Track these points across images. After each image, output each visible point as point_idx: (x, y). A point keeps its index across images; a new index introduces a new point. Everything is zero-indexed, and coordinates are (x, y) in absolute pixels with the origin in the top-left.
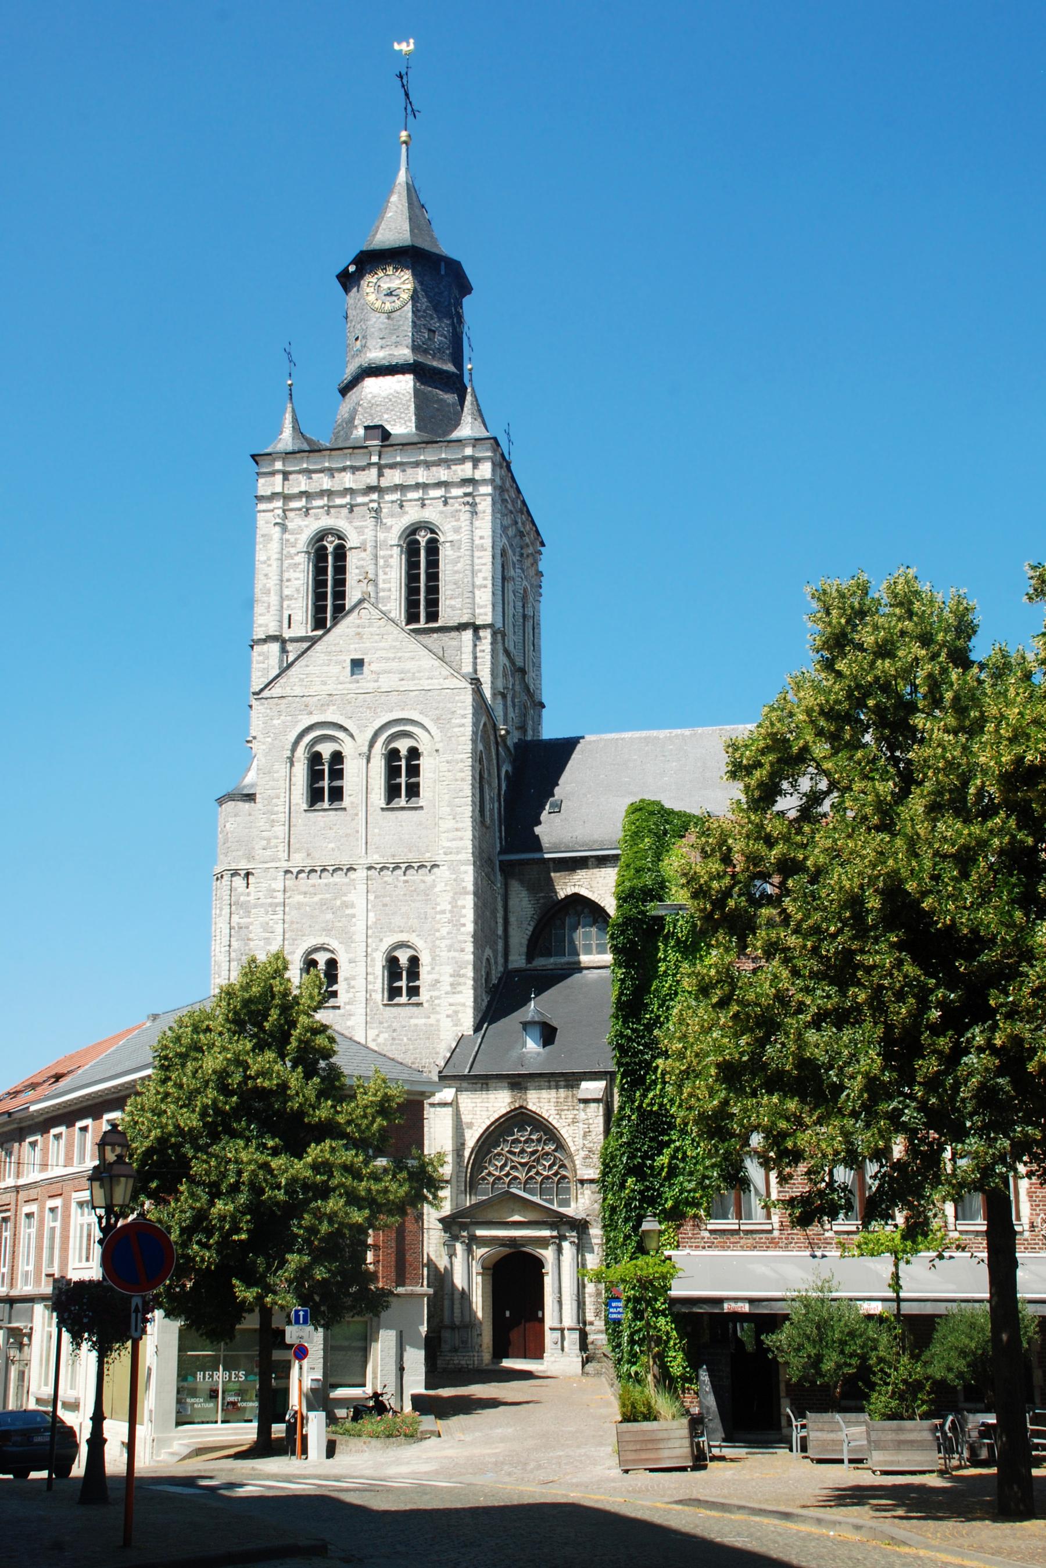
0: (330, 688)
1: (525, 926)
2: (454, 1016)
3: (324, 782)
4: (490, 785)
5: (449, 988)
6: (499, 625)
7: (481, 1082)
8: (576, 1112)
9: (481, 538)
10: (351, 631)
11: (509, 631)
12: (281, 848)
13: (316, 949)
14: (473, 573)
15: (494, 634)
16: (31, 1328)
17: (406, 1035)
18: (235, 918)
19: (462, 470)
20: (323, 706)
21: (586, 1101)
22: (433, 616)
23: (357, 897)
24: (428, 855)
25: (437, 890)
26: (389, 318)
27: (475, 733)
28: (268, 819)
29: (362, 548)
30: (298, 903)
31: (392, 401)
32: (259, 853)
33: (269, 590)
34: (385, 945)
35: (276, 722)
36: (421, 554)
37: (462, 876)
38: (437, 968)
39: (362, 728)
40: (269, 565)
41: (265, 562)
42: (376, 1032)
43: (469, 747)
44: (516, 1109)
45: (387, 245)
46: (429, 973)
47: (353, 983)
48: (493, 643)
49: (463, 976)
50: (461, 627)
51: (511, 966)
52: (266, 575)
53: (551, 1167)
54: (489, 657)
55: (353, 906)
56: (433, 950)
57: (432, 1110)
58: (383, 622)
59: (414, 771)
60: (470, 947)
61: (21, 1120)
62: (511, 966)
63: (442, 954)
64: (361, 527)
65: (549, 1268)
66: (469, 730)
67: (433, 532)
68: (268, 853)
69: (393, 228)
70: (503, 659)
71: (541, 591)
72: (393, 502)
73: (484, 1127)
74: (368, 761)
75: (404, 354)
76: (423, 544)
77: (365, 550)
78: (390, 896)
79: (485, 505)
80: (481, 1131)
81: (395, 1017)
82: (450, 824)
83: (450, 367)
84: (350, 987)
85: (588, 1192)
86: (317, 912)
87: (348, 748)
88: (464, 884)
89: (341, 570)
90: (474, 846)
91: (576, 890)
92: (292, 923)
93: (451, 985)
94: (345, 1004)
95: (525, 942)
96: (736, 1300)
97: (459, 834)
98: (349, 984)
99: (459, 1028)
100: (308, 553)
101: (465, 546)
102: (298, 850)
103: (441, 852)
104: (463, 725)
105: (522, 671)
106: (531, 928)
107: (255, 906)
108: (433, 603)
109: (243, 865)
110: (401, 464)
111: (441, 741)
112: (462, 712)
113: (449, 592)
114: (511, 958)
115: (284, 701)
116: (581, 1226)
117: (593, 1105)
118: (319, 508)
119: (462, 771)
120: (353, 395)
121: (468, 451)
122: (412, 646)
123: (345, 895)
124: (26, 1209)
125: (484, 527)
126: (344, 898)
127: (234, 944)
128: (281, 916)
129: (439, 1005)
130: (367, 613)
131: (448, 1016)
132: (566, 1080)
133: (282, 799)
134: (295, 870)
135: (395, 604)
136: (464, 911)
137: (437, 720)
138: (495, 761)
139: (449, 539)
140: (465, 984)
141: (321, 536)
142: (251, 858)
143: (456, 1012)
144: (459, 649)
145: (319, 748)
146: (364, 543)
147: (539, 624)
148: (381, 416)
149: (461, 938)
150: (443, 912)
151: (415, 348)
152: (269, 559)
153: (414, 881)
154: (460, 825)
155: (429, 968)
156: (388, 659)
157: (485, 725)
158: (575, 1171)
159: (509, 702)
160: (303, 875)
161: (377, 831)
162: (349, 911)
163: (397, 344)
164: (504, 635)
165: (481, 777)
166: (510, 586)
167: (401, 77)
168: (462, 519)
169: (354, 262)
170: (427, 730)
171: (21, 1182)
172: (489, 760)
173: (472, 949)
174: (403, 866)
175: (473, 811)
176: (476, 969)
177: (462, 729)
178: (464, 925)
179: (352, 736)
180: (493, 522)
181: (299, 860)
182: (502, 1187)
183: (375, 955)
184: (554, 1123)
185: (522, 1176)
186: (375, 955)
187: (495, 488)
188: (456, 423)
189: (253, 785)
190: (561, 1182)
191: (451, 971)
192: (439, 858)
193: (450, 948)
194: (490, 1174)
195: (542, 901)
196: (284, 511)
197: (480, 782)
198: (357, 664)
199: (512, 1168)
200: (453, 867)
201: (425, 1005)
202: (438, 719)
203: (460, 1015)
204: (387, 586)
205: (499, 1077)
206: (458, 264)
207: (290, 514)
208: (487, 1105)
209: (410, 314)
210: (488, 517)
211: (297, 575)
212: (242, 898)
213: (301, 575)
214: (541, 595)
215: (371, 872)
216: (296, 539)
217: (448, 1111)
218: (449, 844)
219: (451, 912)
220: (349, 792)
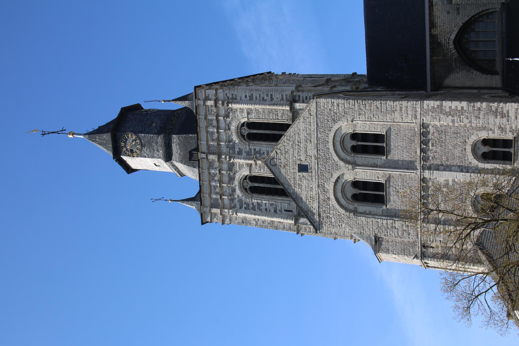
0: (314, 185)
5: (505, 120)
20: (325, 191)
24: (416, 129)
26: (145, 146)
35: (333, 220)
38: (491, 126)
46: (494, 133)
49: (497, 109)
51: (500, 85)
55: (447, 181)
59: (365, 137)
62: (500, 85)
64: (239, 165)
71: (287, 73)
75: (160, 139)
91: (451, 42)
93: (503, 117)
95: (484, 76)
106: (475, 72)
112: (330, 105)
133: (379, 220)
136: (453, 108)
137: (335, 121)
142: (414, 244)
145: (349, 196)
154: (398, 108)
155: (490, 132)
162: (451, 183)
163: (157, 143)
177: (340, 105)
178: (462, 107)
195: (458, 65)
200: (424, 113)
216: (245, 203)
218: (410, 116)
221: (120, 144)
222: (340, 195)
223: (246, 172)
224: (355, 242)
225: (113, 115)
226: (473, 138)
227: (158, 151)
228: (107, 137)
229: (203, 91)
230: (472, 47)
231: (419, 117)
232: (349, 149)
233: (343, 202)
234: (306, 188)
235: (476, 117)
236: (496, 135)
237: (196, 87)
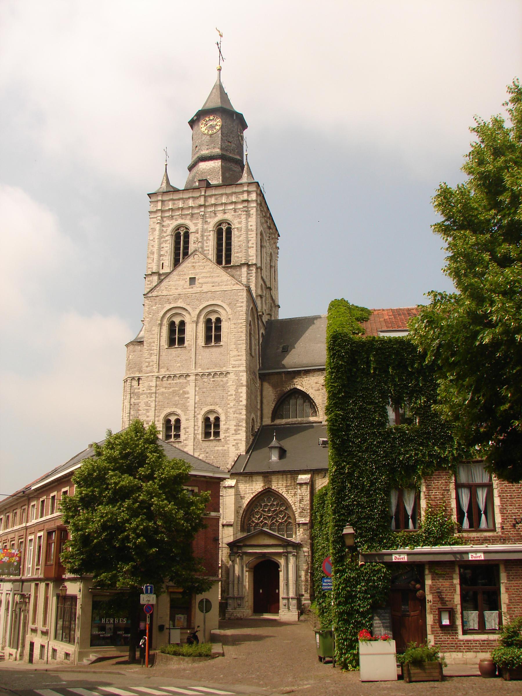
0: (179, 291)
1: (271, 404)
2: (236, 446)
3: (176, 335)
5: (234, 432)
7: (248, 475)
8: (296, 490)
9: (251, 226)
10: (190, 265)
11: (264, 268)
12: (155, 367)
13: (170, 414)
14: (248, 242)
15: (257, 268)
16: (30, 595)
17: (213, 455)
18: (133, 400)
19: (243, 197)
20: (176, 300)
21: (301, 484)
22: (228, 261)
23: (191, 389)
24: (225, 368)
25: (228, 385)
26: (210, 137)
27: (247, 310)
28: (149, 353)
30: (162, 392)
31: (212, 171)
33: (154, 252)
34: (203, 412)
35: (154, 308)
36: (224, 235)
37: (241, 378)
38: (228, 422)
39: (194, 309)
40: (154, 242)
41: (152, 240)
43: (244, 317)
44: (266, 489)
46: (224, 425)
47: (187, 430)
48: (256, 272)
52: (153, 246)
53: (283, 518)
54: (254, 279)
55: (188, 393)
57: (224, 490)
59: (218, 329)
60: (244, 412)
62: (264, 424)
63: (230, 415)
64: (196, 223)
65: (282, 568)
66: (244, 309)
67: (229, 224)
68: (149, 369)
70: (261, 282)
72: (210, 212)
73: (250, 498)
74: (196, 326)
75: (217, 151)
76: (224, 230)
77: (198, 233)
78: (206, 388)
79: (253, 212)
80: (249, 500)
81: (207, 447)
82: (235, 353)
83: (238, 157)
84: (187, 432)
85: (301, 530)
86: (171, 396)
87: (187, 319)
88: (242, 382)
89: (187, 242)
90: (246, 363)
92: (159, 402)
94: (184, 440)
95: (271, 412)
97: (239, 357)
98: (185, 431)
99: (238, 451)
102: (163, 367)
103: (231, 366)
104: (242, 306)
105: (270, 289)
106: (274, 405)
107: (142, 394)
109: (137, 375)
110: (215, 195)
111: (232, 314)
112: (242, 300)
113: (236, 251)
114: (264, 420)
115: (158, 298)
116: (298, 546)
117: (304, 486)
118: (177, 215)
119: (241, 328)
120: (195, 170)
121: (245, 189)
122: (219, 271)
124: (30, 538)
125: (253, 221)
126: (184, 390)
127: (132, 413)
128: (154, 399)
129: (229, 440)
130: (198, 257)
131: (233, 446)
132: (291, 474)
134: (161, 377)
135: (211, 253)
137: (229, 304)
139: (237, 227)
140: (242, 430)
141: (178, 228)
143: (237, 444)
144: (240, 275)
146: (197, 230)
149: (240, 407)
150: (231, 395)
151: (222, 149)
152: (154, 238)
153: (218, 381)
154: (240, 354)
155: (224, 422)
156: (207, 277)
157: (252, 308)
158: (295, 519)
159: (264, 302)
160: (165, 379)
161: (200, 357)
162: (186, 396)
163: (214, 148)
164: (261, 270)
165: (250, 334)
168: (242, 218)
170: (225, 310)
171: (28, 524)
173: (245, 413)
174: (213, 374)
175: (246, 347)
176: (247, 423)
177: (241, 308)
178: (241, 401)
179: (189, 313)
180: (257, 219)
181: (163, 372)
182: (259, 528)
183: (198, 416)
184: (285, 495)
185: (269, 522)
186: (198, 416)
187: (257, 204)
188: (241, 177)
189: (142, 338)
190: (289, 524)
191: (235, 424)
192: (230, 369)
193: (234, 413)
194: (253, 522)
196: (161, 217)
197: (250, 335)
198: (192, 280)
199: (264, 518)
200: (237, 374)
201: (223, 440)
202: (230, 304)
203: (239, 445)
204: (207, 248)
205: (258, 474)
206: (241, 115)
207: (165, 219)
208: (251, 487)
209: (220, 135)
210: (254, 217)
211: (167, 245)
212: (136, 391)
213: (168, 245)
214: (278, 257)
215: (198, 377)
216: (167, 230)
217: (232, 491)
218: (234, 363)
219: (235, 395)
220: (188, 339)
221: (211, 115)
222: (174, 312)
223: (192, 229)
224: (142, 321)
225: (237, 107)
226: (220, 410)
227: (207, 149)
228: (217, 103)
229: (255, 189)
230: (292, 402)
231: (234, 369)
232: (208, 317)
233: (168, 315)
234: (176, 284)
235: (235, 411)
236: (223, 426)
237: (257, 183)
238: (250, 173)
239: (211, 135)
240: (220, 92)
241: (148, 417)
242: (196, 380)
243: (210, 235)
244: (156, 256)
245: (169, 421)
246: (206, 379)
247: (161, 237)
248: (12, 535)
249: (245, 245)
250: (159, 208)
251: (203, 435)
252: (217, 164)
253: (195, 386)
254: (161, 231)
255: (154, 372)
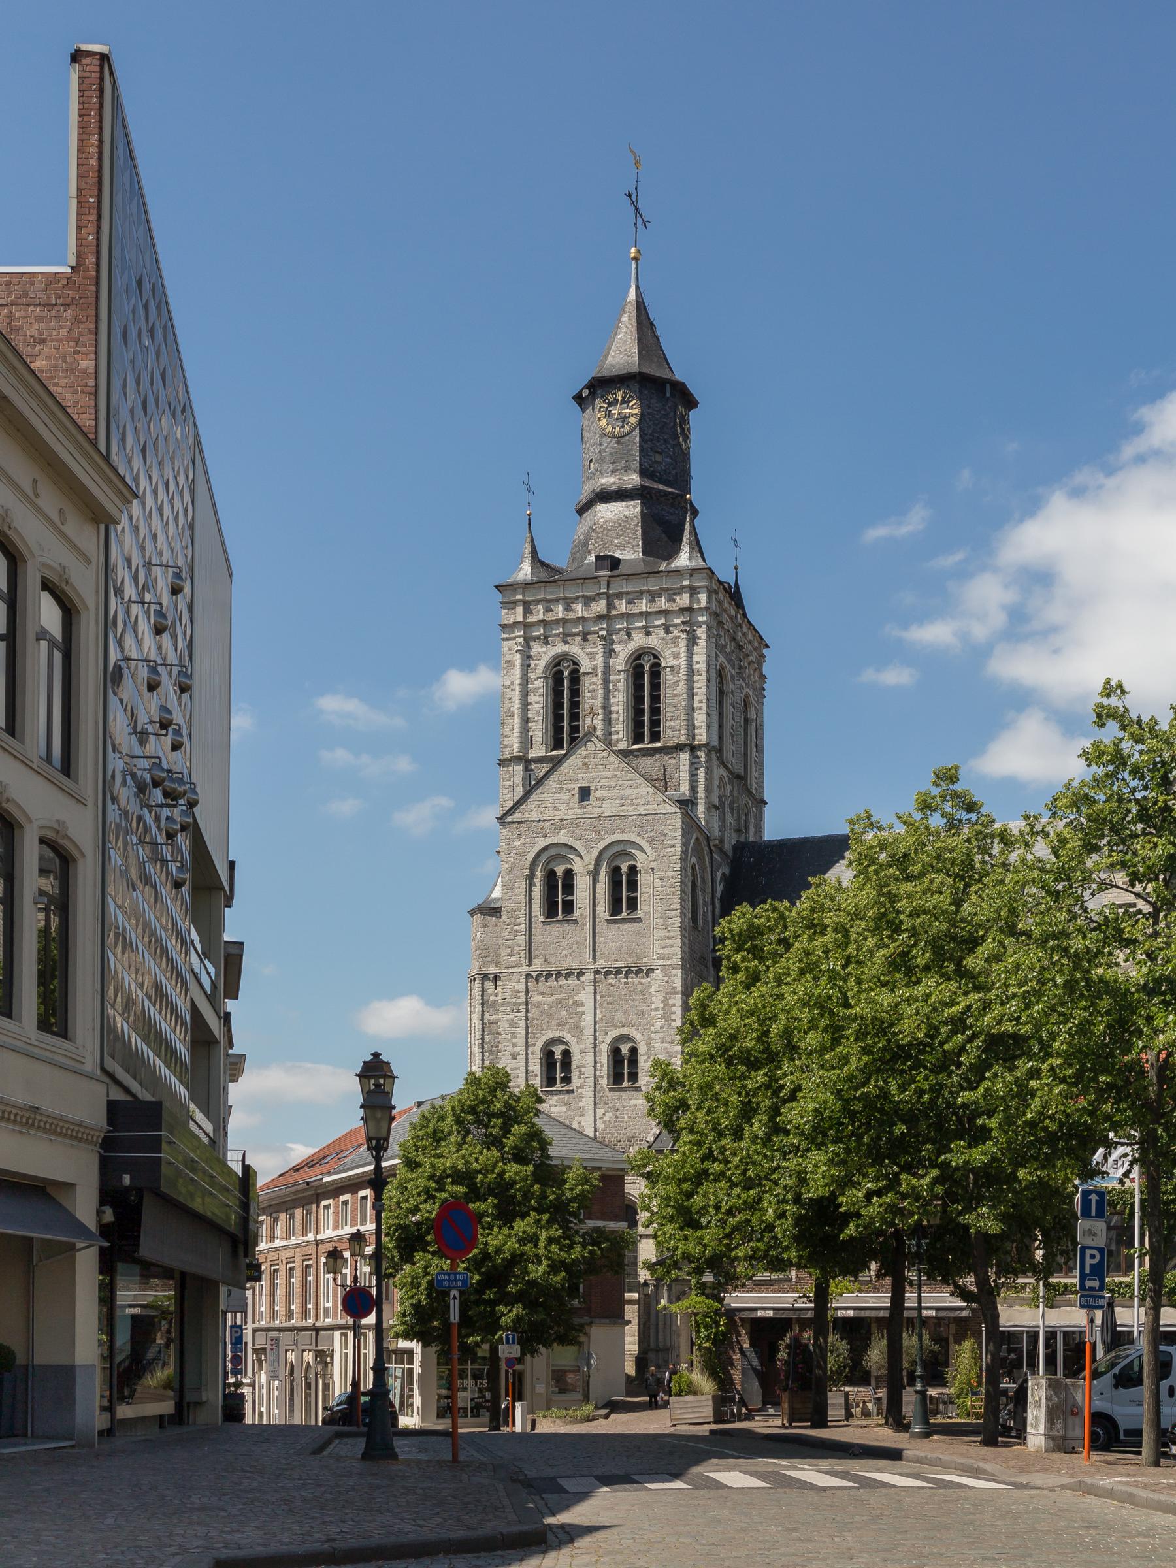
0: (561, 814)
3: (557, 897)
4: (703, 890)
6: (715, 742)
9: (698, 663)
10: (579, 762)
20: (556, 830)
22: (655, 736)
24: (645, 960)
26: (618, 443)
29: (593, 673)
32: (504, 959)
34: (609, 1039)
36: (645, 676)
42: (603, 1111)
45: (615, 372)
46: (645, 1061)
50: (679, 748)
55: (582, 1004)
56: (649, 1042)
58: (605, 754)
59: (633, 885)
61: (317, 1187)
64: (593, 653)
67: (656, 657)
68: (512, 959)
69: (622, 353)
75: (633, 479)
79: (701, 632)
86: (553, 1010)
87: (578, 866)
90: (683, 951)
96: (765, 1309)
100: (546, 678)
101: (683, 671)
102: (537, 956)
107: (503, 1005)
108: (655, 723)
109: (492, 970)
112: (673, 834)
120: (589, 516)
123: (576, 995)
128: (523, 1014)
130: (595, 745)
138: (709, 869)
139: (670, 664)
142: (497, 963)
146: (595, 668)
147: (762, 725)
148: (612, 541)
150: (657, 1009)
151: (643, 473)
152: (512, 683)
154: (671, 934)
162: (579, 1009)
163: (626, 469)
166: (728, 700)
167: (630, 195)
169: (586, 387)
171: (319, 1237)
172: (703, 869)
174: (624, 970)
179: (580, 856)
181: (538, 966)
192: (655, 963)
193: (663, 1040)
200: (666, 971)
202: (653, 840)
206: (683, 384)
215: (600, 977)
218: (662, 951)
222: (552, 852)
223: (585, 666)
226: (638, 1036)
231: (661, 963)
234: (555, 800)
238: (696, 544)
239: (619, 437)
240: (639, 323)
241: (514, 1046)
242: (595, 981)
243: (619, 681)
244: (517, 721)
245: (551, 1053)
246: (612, 980)
247: (525, 681)
248: (289, 1253)
249: (688, 707)
250: (520, 618)
251: (611, 1080)
252: (632, 509)
253: (595, 992)
254: (526, 667)
255: (522, 965)
